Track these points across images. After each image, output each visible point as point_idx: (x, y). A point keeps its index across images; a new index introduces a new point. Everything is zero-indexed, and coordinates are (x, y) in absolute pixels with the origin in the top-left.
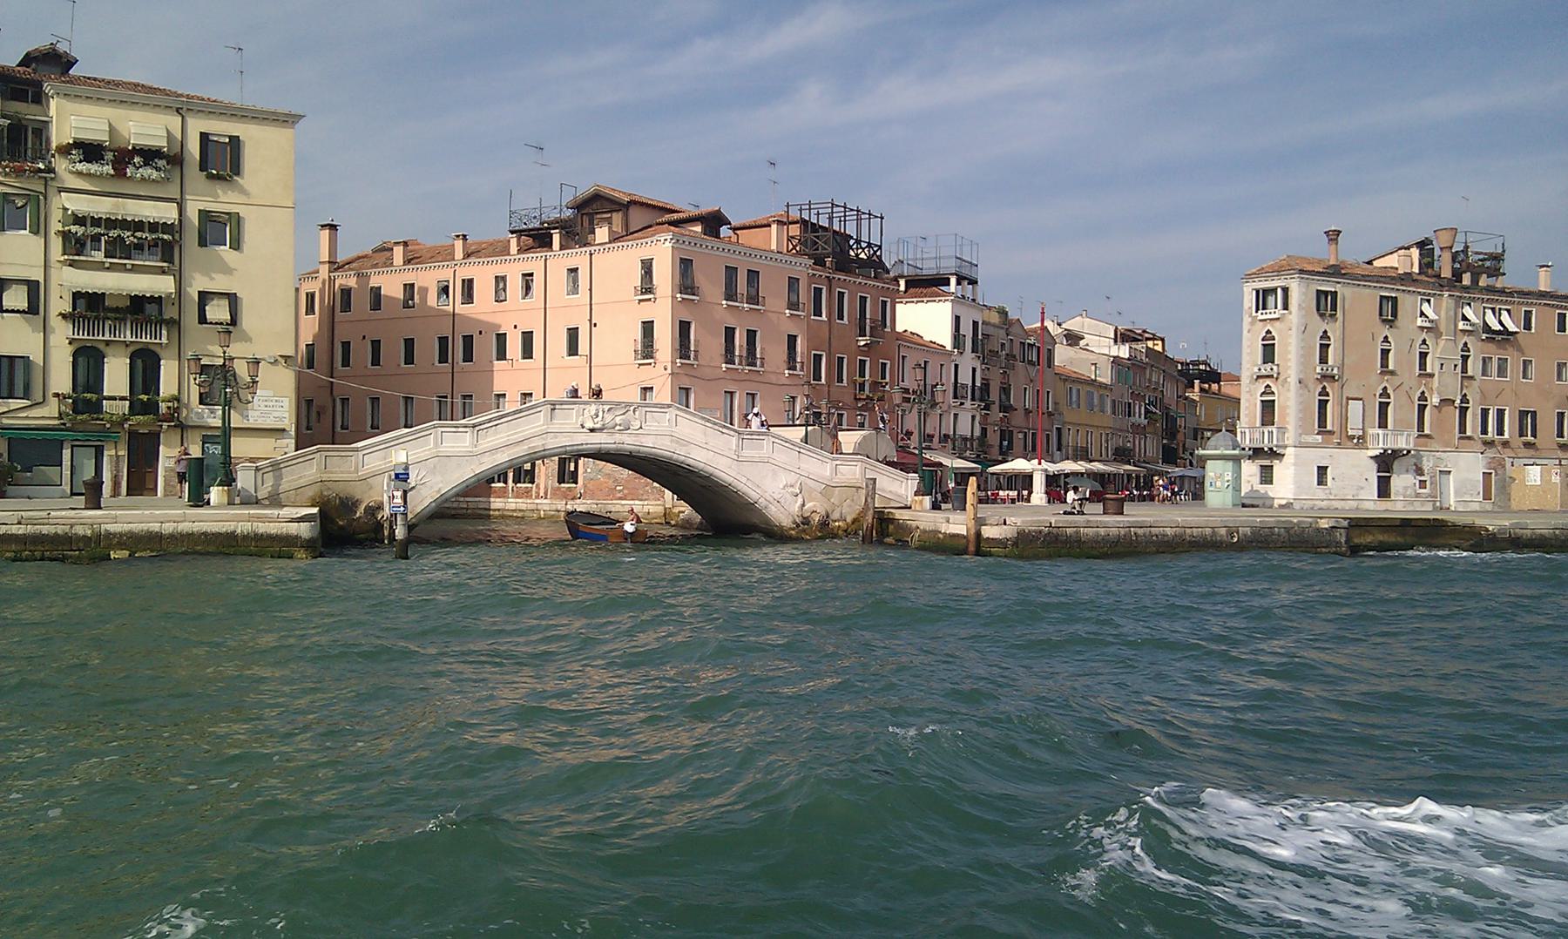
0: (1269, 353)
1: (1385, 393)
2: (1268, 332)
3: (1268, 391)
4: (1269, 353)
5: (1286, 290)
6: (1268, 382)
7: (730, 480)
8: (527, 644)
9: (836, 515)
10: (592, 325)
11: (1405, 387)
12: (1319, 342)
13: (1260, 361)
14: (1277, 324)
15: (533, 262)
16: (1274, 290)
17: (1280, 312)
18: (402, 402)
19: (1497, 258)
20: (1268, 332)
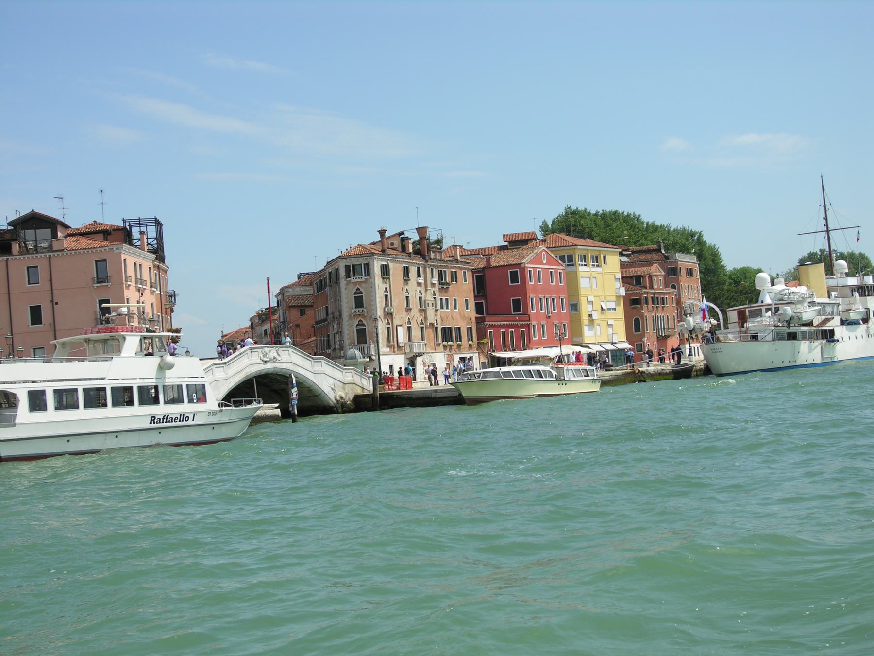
0: (359, 302)
2: (358, 289)
3: (360, 323)
4: (359, 302)
5: (367, 266)
10: (54, 303)
11: (415, 318)
14: (363, 285)
20: (358, 289)
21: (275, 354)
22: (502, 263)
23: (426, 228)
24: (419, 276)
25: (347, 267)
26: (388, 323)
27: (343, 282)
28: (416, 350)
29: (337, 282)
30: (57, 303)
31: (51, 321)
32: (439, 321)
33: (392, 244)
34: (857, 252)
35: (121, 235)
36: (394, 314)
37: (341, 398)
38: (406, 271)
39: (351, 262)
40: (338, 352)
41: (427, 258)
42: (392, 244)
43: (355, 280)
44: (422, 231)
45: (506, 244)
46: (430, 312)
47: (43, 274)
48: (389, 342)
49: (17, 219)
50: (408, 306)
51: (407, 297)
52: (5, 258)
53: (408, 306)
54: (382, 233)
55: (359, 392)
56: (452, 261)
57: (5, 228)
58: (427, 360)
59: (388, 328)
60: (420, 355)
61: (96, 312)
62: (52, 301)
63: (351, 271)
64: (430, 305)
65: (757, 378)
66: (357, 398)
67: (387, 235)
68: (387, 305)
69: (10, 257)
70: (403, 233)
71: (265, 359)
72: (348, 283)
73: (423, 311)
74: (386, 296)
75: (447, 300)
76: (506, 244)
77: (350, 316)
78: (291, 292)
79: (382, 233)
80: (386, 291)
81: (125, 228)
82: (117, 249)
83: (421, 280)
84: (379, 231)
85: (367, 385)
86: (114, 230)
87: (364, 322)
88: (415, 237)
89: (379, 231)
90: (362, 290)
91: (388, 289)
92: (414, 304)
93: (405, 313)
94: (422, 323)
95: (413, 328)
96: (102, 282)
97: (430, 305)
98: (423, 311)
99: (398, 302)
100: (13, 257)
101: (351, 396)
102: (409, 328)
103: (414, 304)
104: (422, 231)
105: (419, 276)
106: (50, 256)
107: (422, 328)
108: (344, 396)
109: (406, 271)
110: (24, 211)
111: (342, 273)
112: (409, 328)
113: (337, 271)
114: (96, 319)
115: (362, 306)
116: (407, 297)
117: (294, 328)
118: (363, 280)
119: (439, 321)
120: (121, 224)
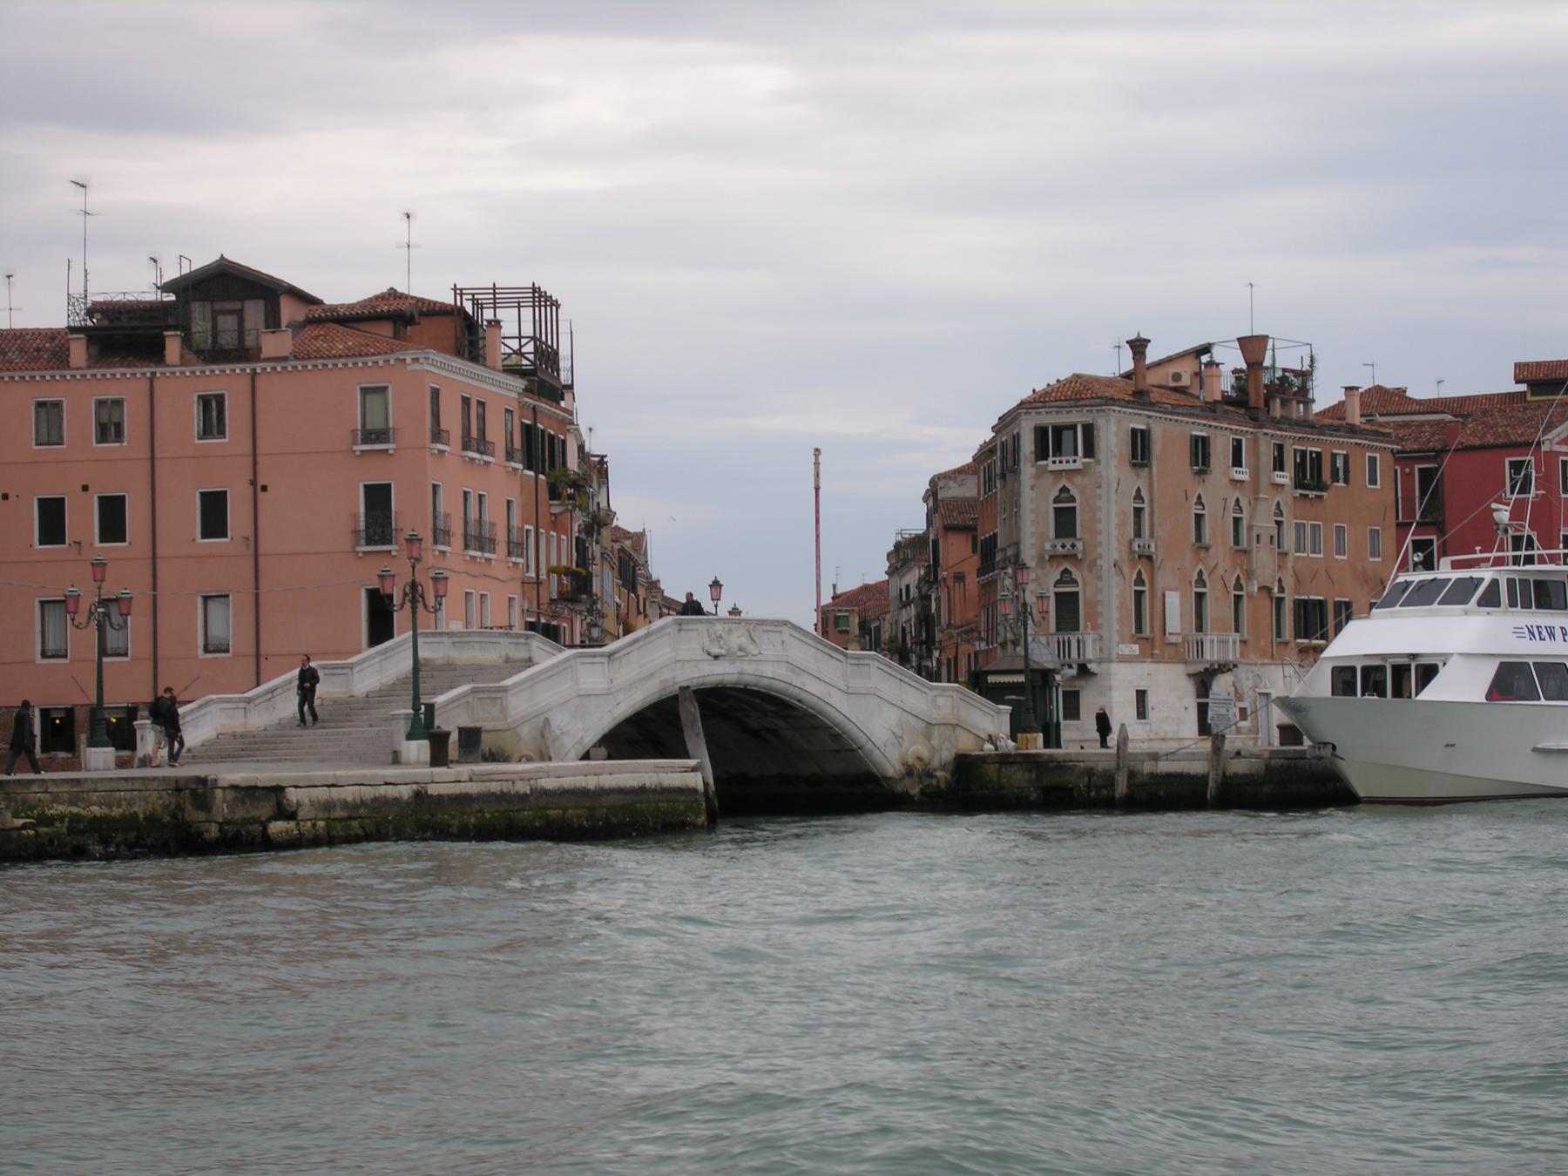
0: (1065, 521)
1: (1201, 582)
2: (1064, 489)
3: (1066, 578)
4: (1065, 521)
5: (1089, 430)
6: (1066, 565)
7: (839, 718)
8: (255, 923)
9: (936, 763)
10: (258, 488)
11: (1220, 571)
12: (1052, 506)
13: (1052, 533)
14: (1078, 479)
15: (125, 383)
16: (1073, 427)
17: (1081, 461)
18: (200, 600)
19: (1305, 375)
20: (1064, 489)
21: (744, 641)
22: (1490, 440)
23: (1266, 338)
24: (1237, 462)
25: (1041, 432)
26: (1139, 581)
27: (1027, 469)
28: (1212, 655)
29: (1016, 471)
30: (264, 488)
31: (249, 532)
32: (1289, 582)
33: (1177, 377)
34: (1053, 382)
35: (447, 327)
36: (1158, 560)
37: (919, 759)
38: (1200, 451)
39: (1050, 419)
40: (1010, 647)
41: (1262, 416)
42: (1177, 377)
43: (1058, 467)
44: (1253, 346)
45: (1523, 387)
46: (1264, 559)
47: (235, 415)
48: (1139, 628)
49: (183, 278)
50: (1199, 538)
51: (1199, 517)
52: (148, 371)
53: (1199, 538)
54: (1138, 346)
55: (966, 744)
56: (1338, 429)
57: (151, 296)
58: (1246, 685)
59: (1139, 594)
60: (1223, 668)
61: (356, 515)
62: (254, 483)
63: (1050, 441)
64: (1265, 539)
65: (262, 591)
66: (964, 765)
67: (1152, 355)
68: (1138, 534)
69: (159, 370)
70: (1206, 349)
71: (716, 650)
72: (1042, 472)
73: (1242, 553)
74: (1138, 512)
75: (1315, 528)
76: (1523, 387)
77: (1040, 557)
78: (952, 491)
79: (1138, 346)
80: (1138, 496)
81: (462, 310)
82: (416, 360)
83: (1242, 474)
84: (1130, 342)
85: (987, 725)
86: (422, 314)
87: (1076, 575)
88: (1231, 360)
89: (1130, 342)
90: (1074, 492)
91: (1144, 494)
92: (1217, 530)
93: (1189, 557)
94: (1238, 586)
95: (1208, 600)
96: (378, 440)
97: (1265, 539)
98: (1242, 553)
99: (1169, 529)
100: (168, 370)
101: (947, 755)
102: (1200, 597)
103: (1217, 530)
104: (1253, 346)
105: (1237, 462)
106: (153, 374)
107: (1238, 598)
108: (925, 754)
109: (1200, 451)
110: (202, 259)
111: (1028, 445)
112: (1200, 597)
113: (1016, 439)
114: (356, 532)
115: (1073, 534)
116: (1199, 517)
117: (950, 582)
118: (1078, 465)
119: (1289, 582)
120: (448, 298)
